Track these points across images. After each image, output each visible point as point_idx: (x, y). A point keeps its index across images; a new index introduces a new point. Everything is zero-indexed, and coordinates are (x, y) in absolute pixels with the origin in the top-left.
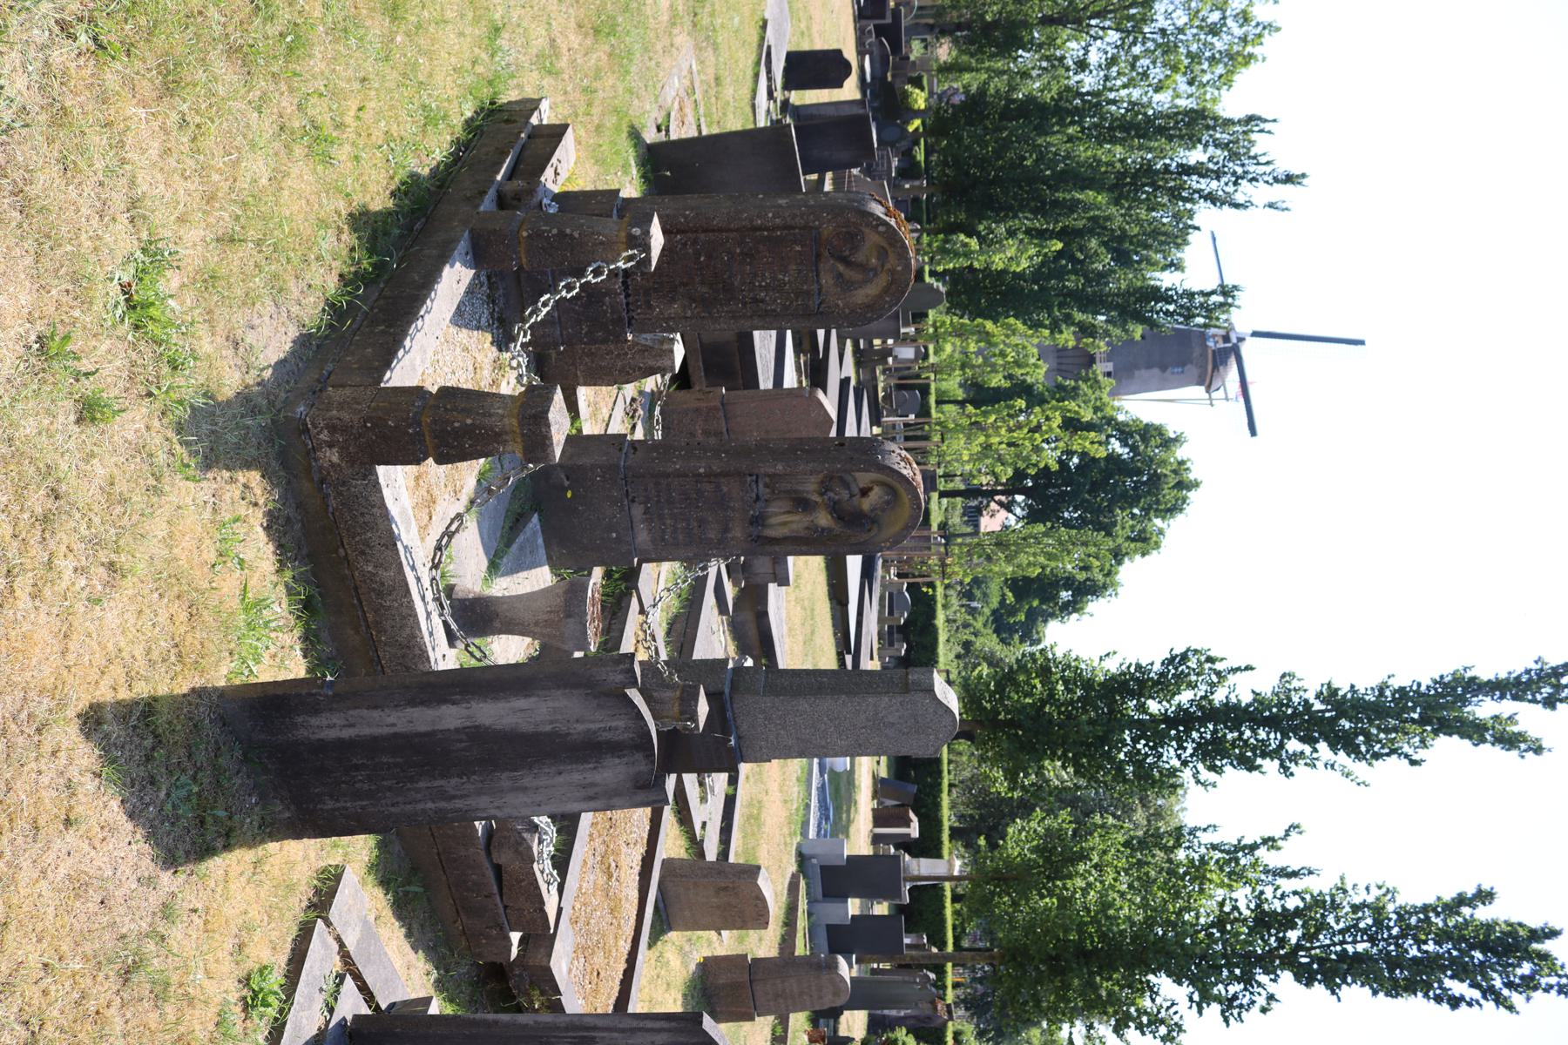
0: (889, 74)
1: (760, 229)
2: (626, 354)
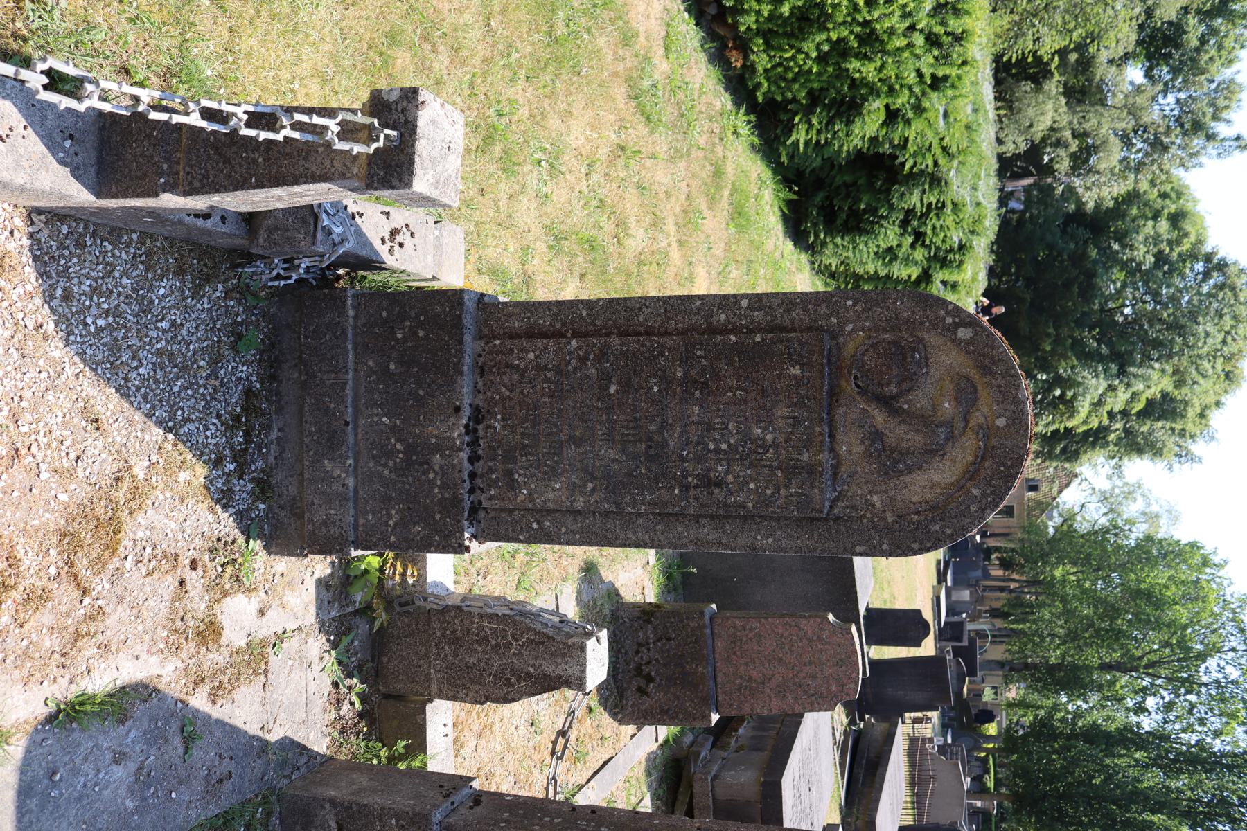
0: (965, 690)
1: (724, 330)
2: (509, 646)
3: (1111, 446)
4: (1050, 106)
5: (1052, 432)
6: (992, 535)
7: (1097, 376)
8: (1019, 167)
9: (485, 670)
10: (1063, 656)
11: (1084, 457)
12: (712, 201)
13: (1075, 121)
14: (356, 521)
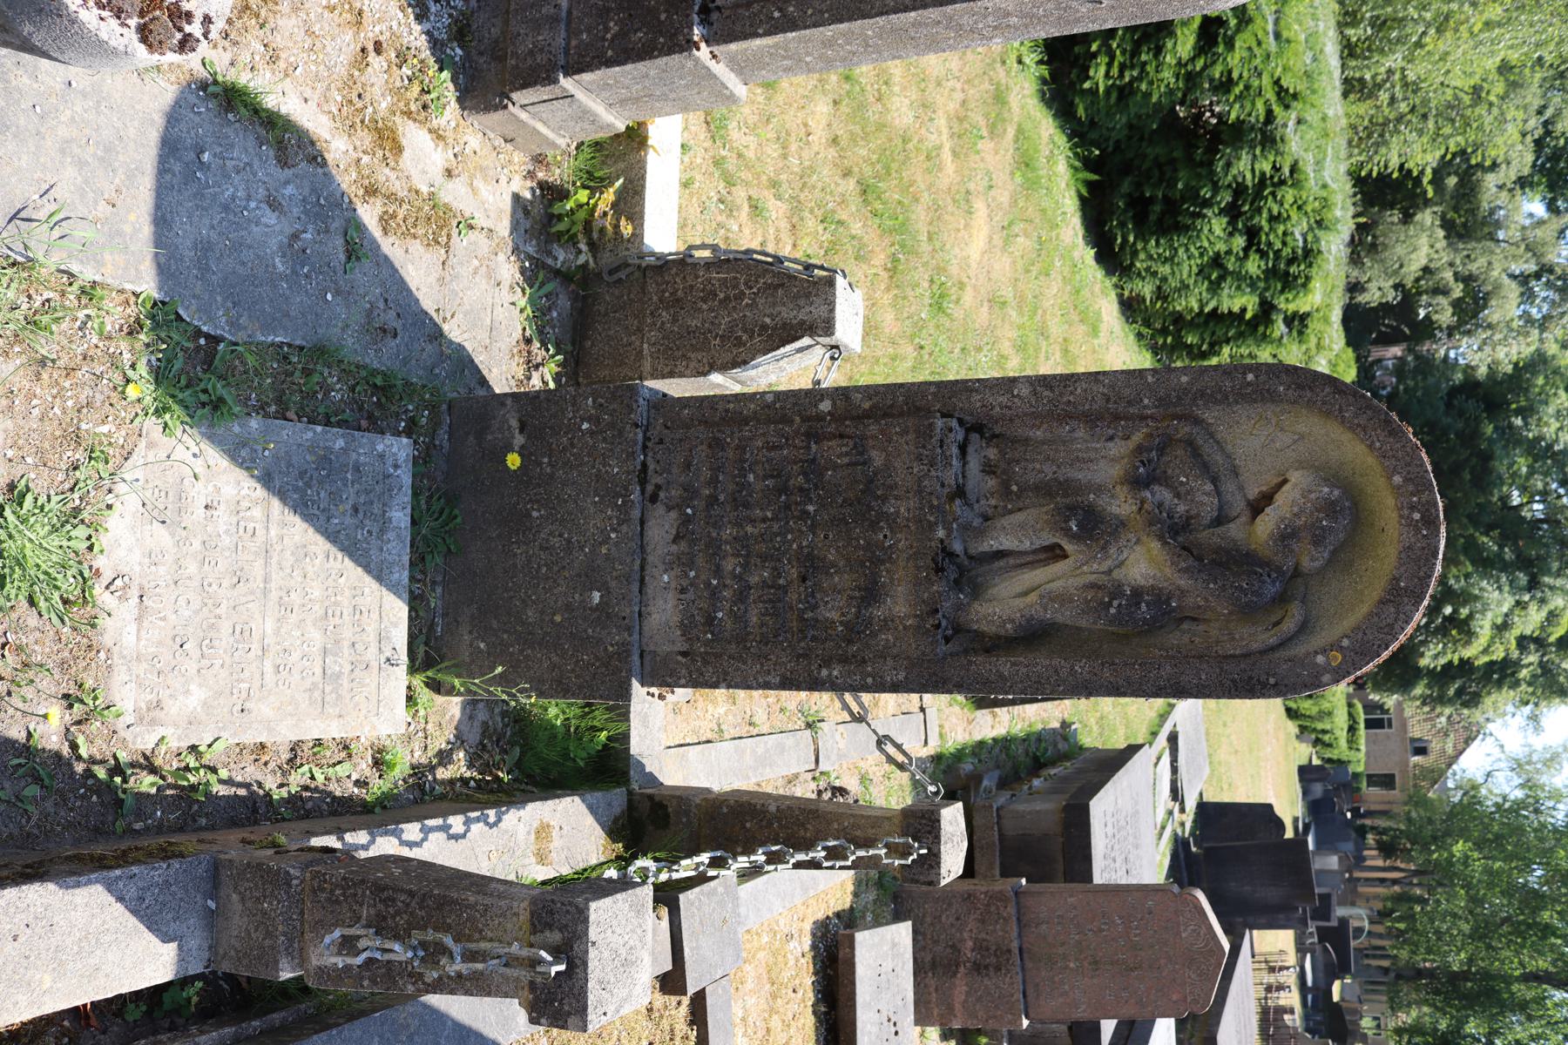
3: (1524, 687)
4: (1424, 241)
5: (1443, 666)
6: (1369, 814)
7: (1500, 588)
8: (1387, 326)
9: (710, 331)
10: (1470, 961)
11: (1488, 701)
12: (994, 131)
13: (1458, 262)
14: (568, 44)
